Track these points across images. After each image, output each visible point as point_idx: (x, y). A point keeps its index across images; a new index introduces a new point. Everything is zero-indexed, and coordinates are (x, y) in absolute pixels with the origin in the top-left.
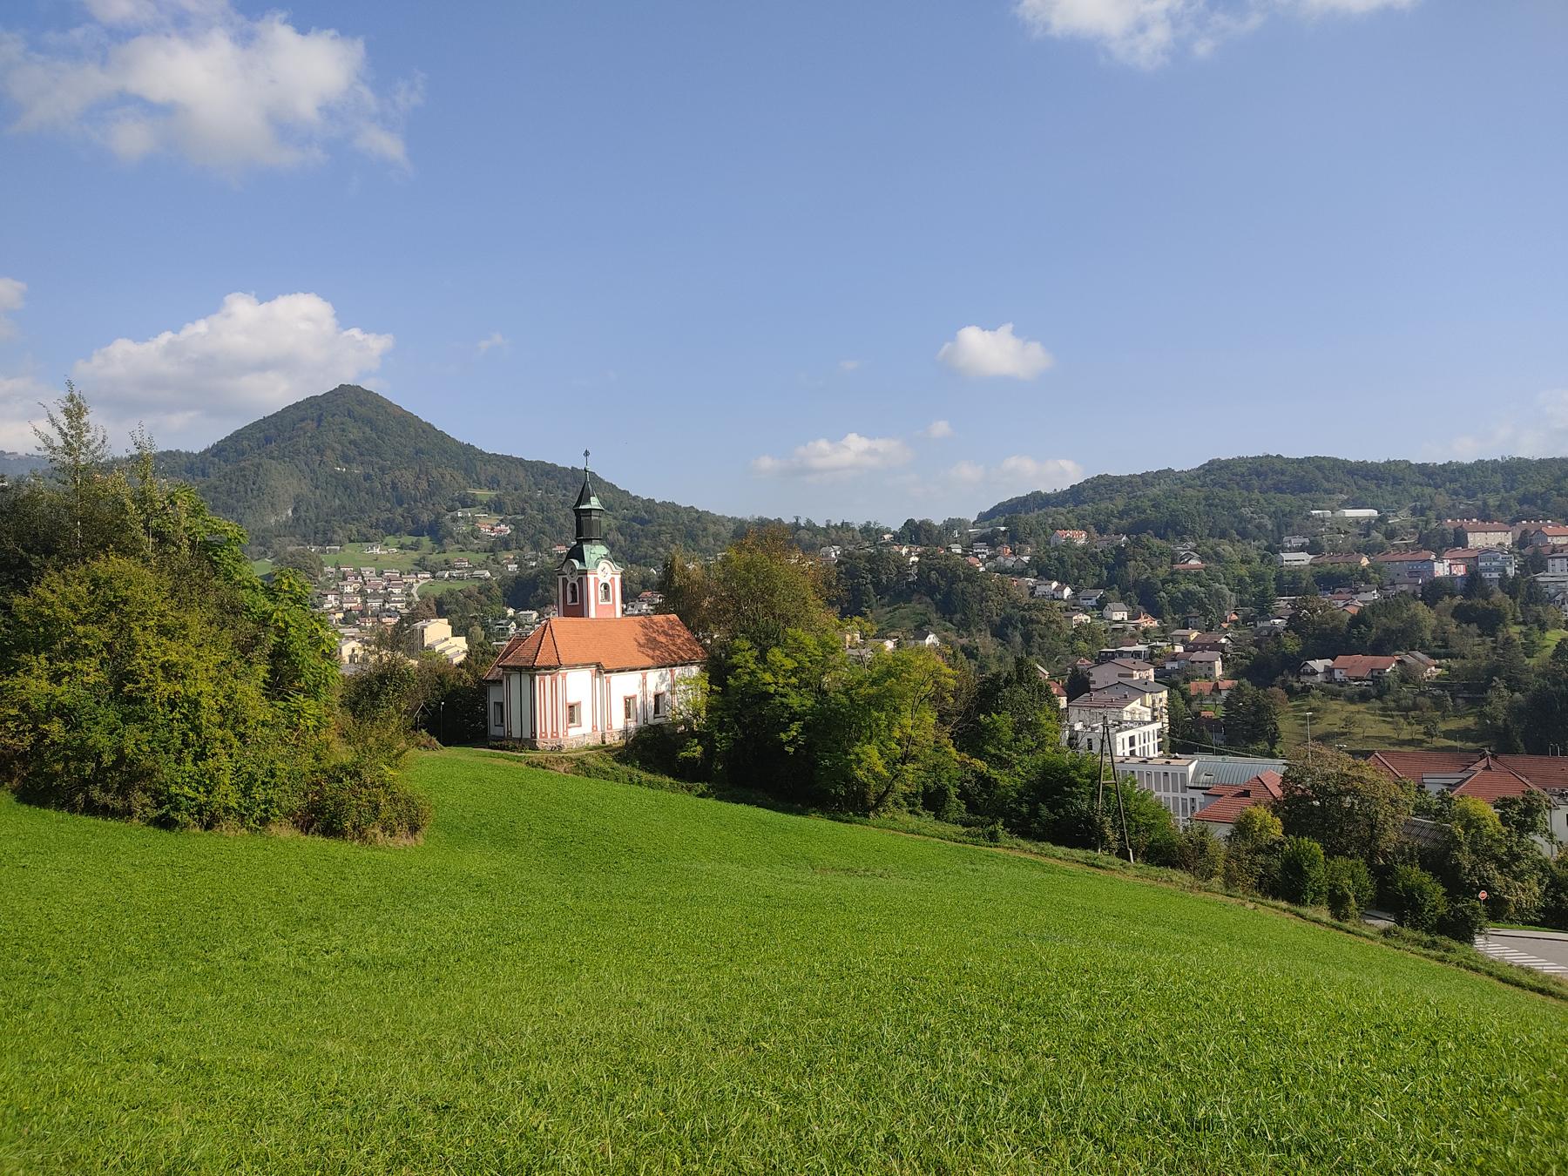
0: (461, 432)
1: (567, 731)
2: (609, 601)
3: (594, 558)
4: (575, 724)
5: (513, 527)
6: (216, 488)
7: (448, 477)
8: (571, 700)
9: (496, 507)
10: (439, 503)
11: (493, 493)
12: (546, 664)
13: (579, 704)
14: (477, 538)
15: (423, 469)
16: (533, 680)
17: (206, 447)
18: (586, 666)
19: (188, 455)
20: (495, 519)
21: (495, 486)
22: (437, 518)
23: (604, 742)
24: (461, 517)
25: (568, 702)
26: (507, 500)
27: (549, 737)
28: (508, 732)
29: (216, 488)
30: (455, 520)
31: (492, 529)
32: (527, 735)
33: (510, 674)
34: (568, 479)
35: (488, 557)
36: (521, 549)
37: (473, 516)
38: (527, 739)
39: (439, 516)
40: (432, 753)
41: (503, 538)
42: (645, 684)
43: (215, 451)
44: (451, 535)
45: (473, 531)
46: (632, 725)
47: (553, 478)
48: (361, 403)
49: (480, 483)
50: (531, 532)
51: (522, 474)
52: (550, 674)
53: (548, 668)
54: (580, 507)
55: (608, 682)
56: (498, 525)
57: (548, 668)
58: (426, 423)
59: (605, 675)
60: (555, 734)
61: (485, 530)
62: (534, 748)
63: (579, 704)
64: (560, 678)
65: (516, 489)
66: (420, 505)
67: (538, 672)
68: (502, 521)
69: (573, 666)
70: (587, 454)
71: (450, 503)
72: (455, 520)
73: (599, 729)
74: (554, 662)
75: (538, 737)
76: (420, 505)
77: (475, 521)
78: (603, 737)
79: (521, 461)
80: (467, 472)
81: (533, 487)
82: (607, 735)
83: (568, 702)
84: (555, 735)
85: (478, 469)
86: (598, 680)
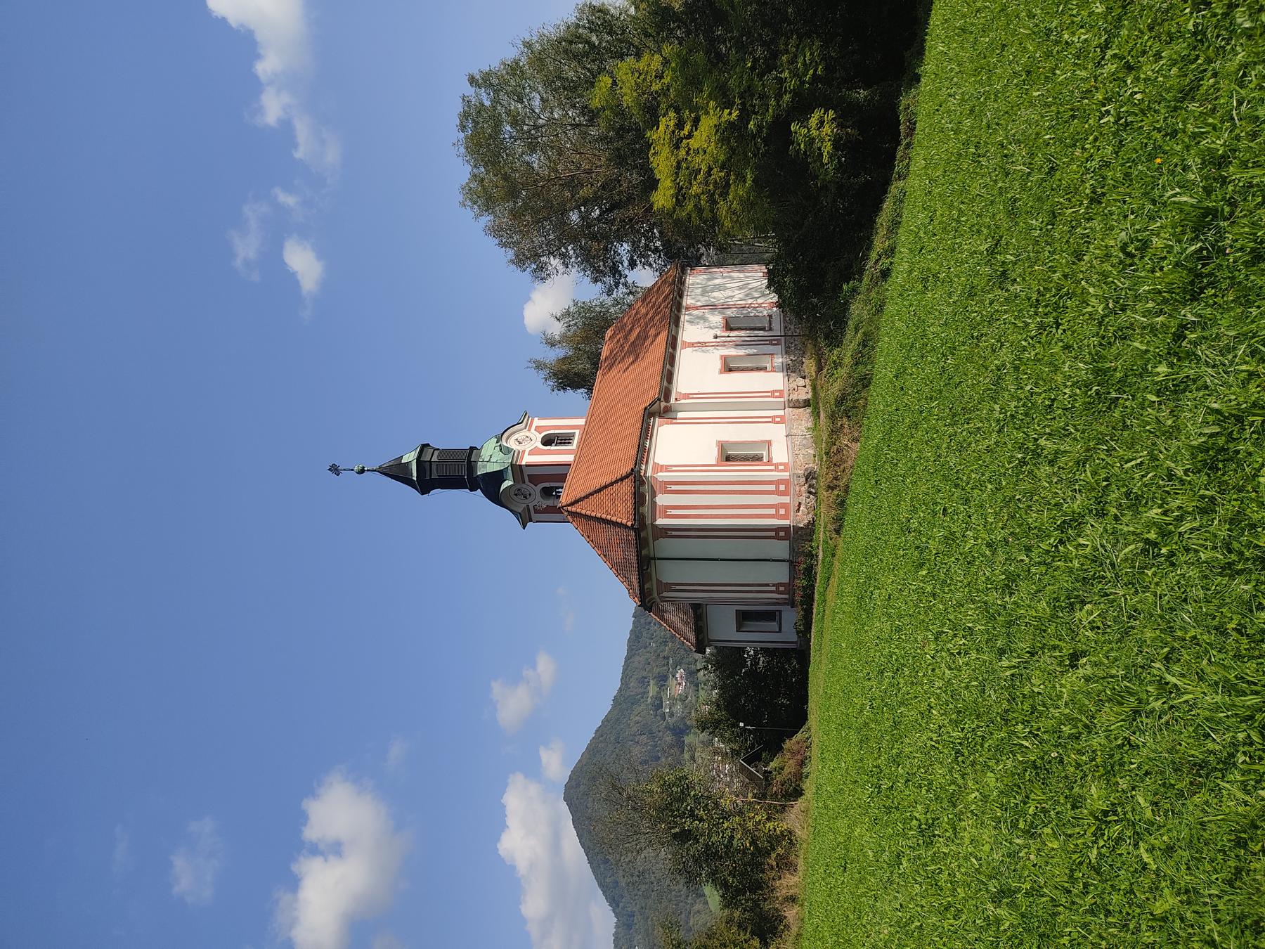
0: (604, 706)
1: (777, 465)
2: (573, 435)
3: (498, 456)
4: (765, 454)
5: (679, 667)
6: (642, 908)
7: (637, 718)
8: (712, 456)
9: (662, 680)
10: (658, 726)
11: (652, 682)
12: (630, 504)
13: (722, 446)
14: (687, 697)
15: (631, 738)
16: (666, 532)
17: (611, 912)
18: (646, 433)
19: (617, 927)
20: (671, 681)
21: (646, 680)
22: (670, 729)
23: (807, 403)
24: (670, 709)
25: (714, 462)
26: (656, 670)
27: (786, 499)
28: (777, 592)
29: (642, 908)
30: (671, 715)
31: (680, 684)
32: (781, 549)
33: (659, 582)
34: (642, 621)
35: (702, 689)
36: (696, 661)
37: (669, 699)
38: (792, 549)
39: (668, 728)
40: (815, 752)
41: (686, 675)
42: (702, 345)
43: (614, 905)
44: (683, 719)
45: (681, 700)
46: (779, 360)
47: (641, 633)
48: (578, 785)
49: (644, 693)
50: (682, 652)
51: (637, 658)
52: (654, 495)
53: (639, 499)
54: (415, 479)
55: (687, 396)
56: (676, 679)
57: (639, 499)
58: (596, 733)
59: (673, 401)
60: (780, 487)
61: (680, 690)
62: (806, 533)
63: (722, 446)
64: (662, 476)
65: (649, 664)
66: (659, 742)
67: (648, 522)
68: (673, 676)
69: (642, 452)
70: (335, 469)
71: (658, 718)
72: (671, 715)
73: (781, 413)
74: (627, 487)
75: (786, 522)
76: (659, 742)
77: (672, 698)
78: (796, 405)
79: (627, 659)
80: (635, 703)
81: (648, 649)
82: (794, 397)
83: (714, 462)
84: (782, 488)
85: (632, 693)
86: (680, 415)
